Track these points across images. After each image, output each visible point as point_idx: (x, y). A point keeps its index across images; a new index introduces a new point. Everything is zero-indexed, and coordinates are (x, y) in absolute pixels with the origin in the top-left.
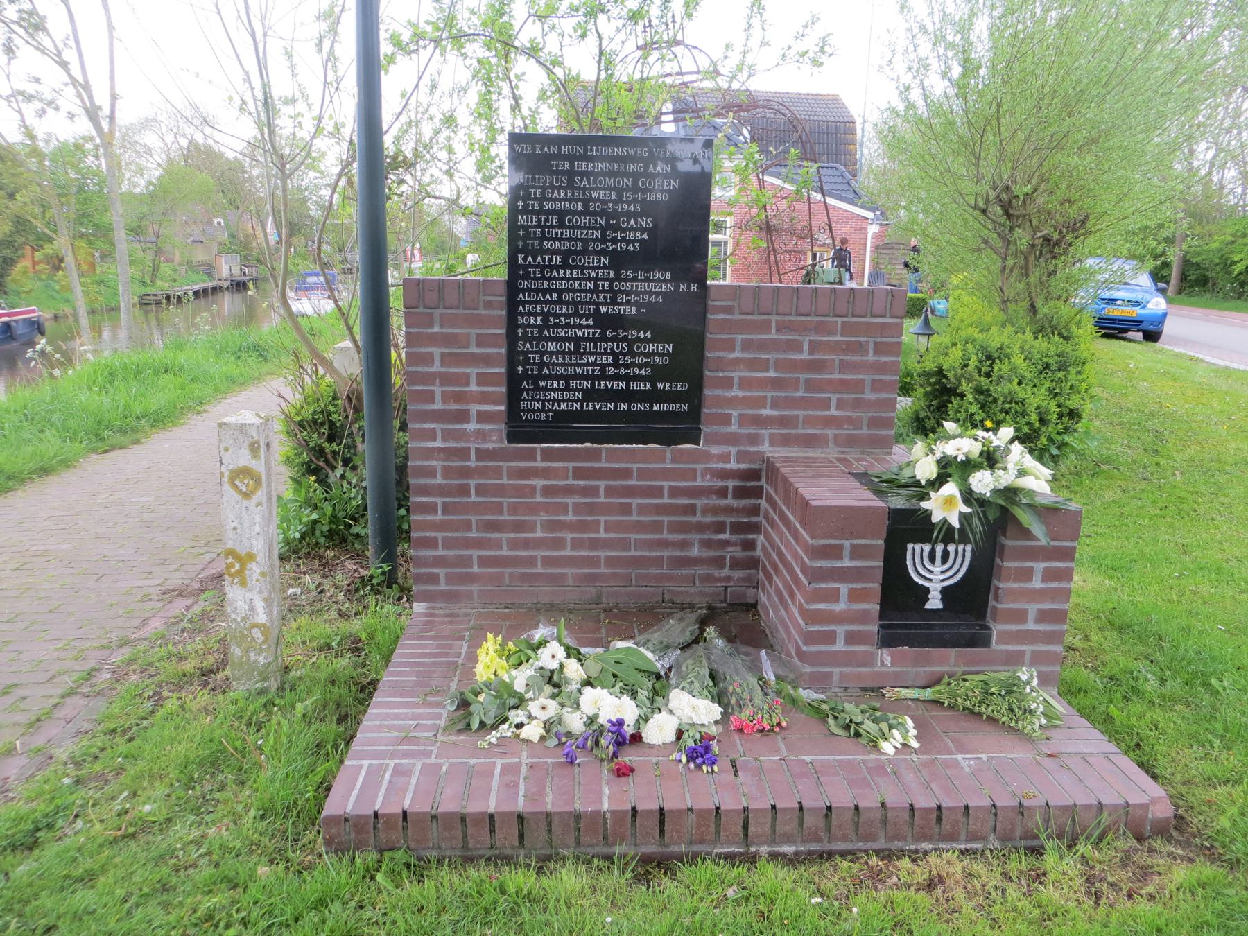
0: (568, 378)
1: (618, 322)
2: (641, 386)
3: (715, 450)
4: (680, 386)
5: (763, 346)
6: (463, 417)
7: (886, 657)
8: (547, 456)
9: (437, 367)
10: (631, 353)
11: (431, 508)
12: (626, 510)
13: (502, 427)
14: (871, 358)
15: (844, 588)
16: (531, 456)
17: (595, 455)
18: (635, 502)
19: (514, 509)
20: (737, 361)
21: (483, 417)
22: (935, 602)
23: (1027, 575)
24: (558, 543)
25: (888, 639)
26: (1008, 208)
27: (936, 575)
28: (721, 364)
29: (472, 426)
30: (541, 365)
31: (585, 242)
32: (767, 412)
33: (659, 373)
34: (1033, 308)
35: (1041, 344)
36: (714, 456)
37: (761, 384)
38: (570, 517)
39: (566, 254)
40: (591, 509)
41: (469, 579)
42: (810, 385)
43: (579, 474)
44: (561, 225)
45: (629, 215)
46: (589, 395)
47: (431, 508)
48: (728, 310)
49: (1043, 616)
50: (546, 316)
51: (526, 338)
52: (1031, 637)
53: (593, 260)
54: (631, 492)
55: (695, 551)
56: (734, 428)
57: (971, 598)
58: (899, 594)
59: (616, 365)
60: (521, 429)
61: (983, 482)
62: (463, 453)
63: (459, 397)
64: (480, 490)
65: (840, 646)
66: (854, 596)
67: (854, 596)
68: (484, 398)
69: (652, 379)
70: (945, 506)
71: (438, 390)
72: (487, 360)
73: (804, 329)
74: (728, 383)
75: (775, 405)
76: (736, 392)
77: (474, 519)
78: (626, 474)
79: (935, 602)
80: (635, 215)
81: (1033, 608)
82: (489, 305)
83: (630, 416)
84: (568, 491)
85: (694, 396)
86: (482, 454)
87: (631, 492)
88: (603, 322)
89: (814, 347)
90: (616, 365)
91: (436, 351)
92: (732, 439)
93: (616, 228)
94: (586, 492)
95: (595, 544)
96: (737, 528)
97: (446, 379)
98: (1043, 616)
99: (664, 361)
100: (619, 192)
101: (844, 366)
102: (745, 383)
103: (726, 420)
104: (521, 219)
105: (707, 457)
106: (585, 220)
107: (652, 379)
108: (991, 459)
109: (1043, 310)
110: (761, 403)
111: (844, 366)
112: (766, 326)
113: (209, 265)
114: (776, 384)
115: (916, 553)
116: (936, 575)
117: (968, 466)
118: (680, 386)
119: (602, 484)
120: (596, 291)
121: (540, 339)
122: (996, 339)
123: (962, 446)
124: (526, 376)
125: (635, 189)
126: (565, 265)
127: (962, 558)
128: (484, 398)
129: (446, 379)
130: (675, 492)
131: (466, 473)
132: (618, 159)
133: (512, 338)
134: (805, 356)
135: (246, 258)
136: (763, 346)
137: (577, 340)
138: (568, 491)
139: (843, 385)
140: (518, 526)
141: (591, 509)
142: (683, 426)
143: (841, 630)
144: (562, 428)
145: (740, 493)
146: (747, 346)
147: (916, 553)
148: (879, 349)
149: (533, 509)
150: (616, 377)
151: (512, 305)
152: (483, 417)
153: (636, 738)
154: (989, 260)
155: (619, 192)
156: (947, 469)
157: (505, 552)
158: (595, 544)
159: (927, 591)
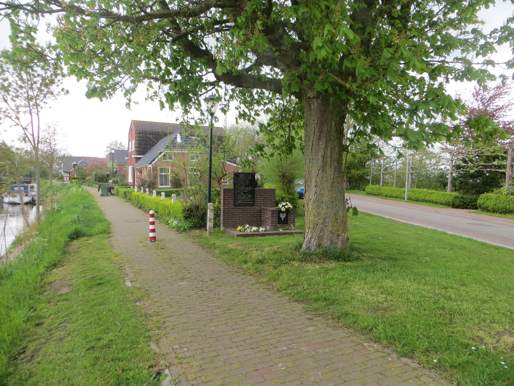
1: (246, 193)
6: (229, 204)
7: (279, 225)
25: (279, 223)
26: (283, 176)
27: (283, 216)
28: (257, 197)
34: (288, 191)
35: (290, 196)
36: (257, 208)
41: (229, 224)
57: (286, 219)
58: (280, 219)
61: (286, 207)
70: (283, 209)
85: (254, 201)
88: (244, 193)
92: (258, 206)
96: (260, 217)
97: (227, 200)
108: (287, 205)
109: (290, 191)
115: (281, 214)
116: (283, 216)
117: (285, 206)
122: (283, 195)
123: (284, 204)
127: (285, 214)
129: (227, 200)
131: (229, 211)
139: (270, 200)
142: (253, 205)
144: (240, 205)
145: (260, 212)
147: (281, 214)
151: (234, 191)
154: (281, 183)
156: (283, 206)
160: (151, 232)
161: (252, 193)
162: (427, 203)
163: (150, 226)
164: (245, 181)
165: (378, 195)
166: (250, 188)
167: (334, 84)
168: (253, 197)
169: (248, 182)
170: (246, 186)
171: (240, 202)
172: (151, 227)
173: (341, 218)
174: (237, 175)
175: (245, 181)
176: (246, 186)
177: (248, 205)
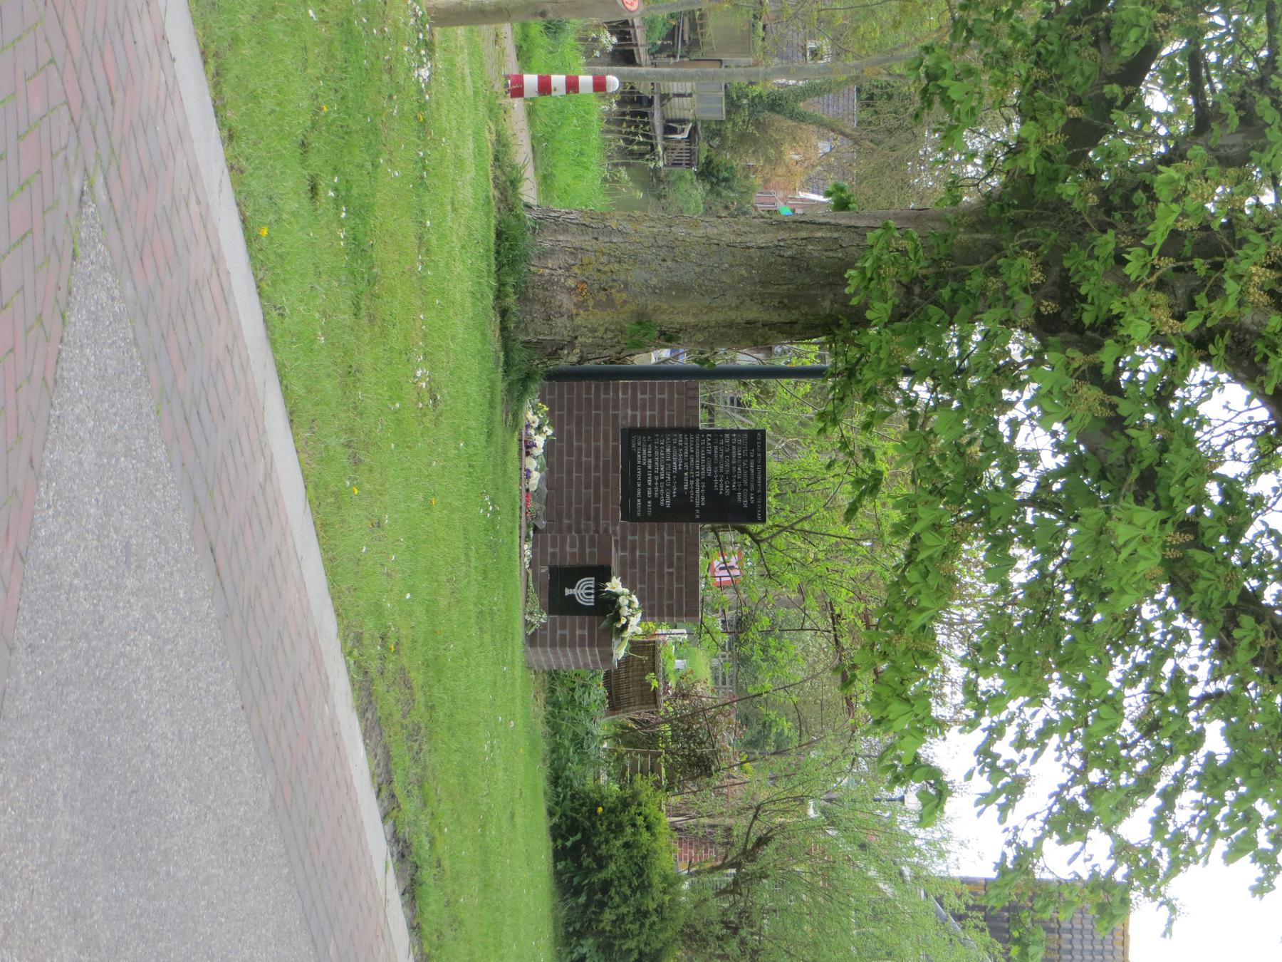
0: (653, 457)
1: (680, 481)
2: (649, 493)
3: (618, 528)
4: (650, 512)
5: (670, 548)
6: (634, 408)
7: (545, 570)
8: (615, 448)
9: (658, 396)
10: (665, 488)
11: (588, 392)
12: (588, 486)
13: (629, 425)
14: (665, 603)
15: (576, 550)
16: (615, 440)
17: (615, 471)
18: (592, 491)
19: (588, 432)
20: (662, 537)
21: (634, 417)
22: (568, 592)
23: (582, 628)
24: (570, 454)
25: (553, 570)
29: (629, 412)
30: (659, 446)
31: (718, 465)
32: (638, 553)
33: (656, 501)
37: (652, 549)
38: (584, 459)
39: (712, 456)
40: (588, 470)
42: (651, 574)
43: (606, 464)
44: (725, 454)
45: (731, 485)
46: (644, 469)
47: (588, 392)
48: (687, 531)
49: (563, 636)
50: (683, 447)
51: (672, 438)
52: (570, 444)
53: (709, 469)
54: (597, 488)
55: (566, 521)
56: (630, 538)
59: (660, 481)
60: (630, 434)
62: (616, 407)
63: (644, 406)
64: (598, 416)
65: (550, 550)
66: (573, 554)
67: (573, 554)
68: (643, 418)
69: (653, 498)
71: (647, 396)
72: (662, 419)
73: (679, 569)
74: (652, 534)
75: (642, 557)
76: (647, 538)
77: (583, 412)
78: (606, 486)
79: (568, 592)
80: (731, 488)
81: (567, 632)
82: (688, 420)
83: (635, 480)
84: (597, 458)
85: (644, 518)
86: (616, 416)
87: (597, 488)
88: (680, 473)
89: (670, 574)
90: (660, 481)
91: (666, 396)
93: (725, 479)
94: (597, 466)
95: (570, 472)
97: (652, 400)
98: (563, 636)
99: (662, 503)
100: (741, 480)
101: (661, 590)
102: (652, 542)
103: (634, 534)
104: (727, 436)
105: (615, 523)
106: (728, 465)
107: (653, 498)
110: (642, 549)
111: (661, 590)
112: (680, 550)
113: (695, 44)
114: (652, 559)
115: (589, 582)
116: (582, 591)
118: (650, 512)
119: (601, 474)
120: (695, 470)
121: (672, 444)
124: (654, 438)
125: (743, 487)
126: (707, 456)
127: (590, 601)
128: (643, 418)
129: (652, 400)
130: (597, 510)
131: (606, 409)
132: (756, 480)
133: (672, 430)
134: (666, 570)
135: (715, 131)
136: (670, 548)
137: (671, 462)
138: (597, 458)
140: (579, 433)
141: (588, 470)
142: (629, 515)
143: (558, 550)
144: (629, 456)
146: (671, 542)
148: (670, 607)
149: (588, 441)
150: (653, 481)
152: (634, 417)
153: (528, 454)
155: (741, 480)
157: (566, 427)
158: (570, 472)
159: (573, 587)
160: (540, 78)
161: (682, 511)
162: (541, 728)
163: (563, 78)
164: (729, 477)
165: (267, 328)
166: (700, 501)
167: (41, 852)
168: (660, 515)
169: (723, 488)
170: (709, 481)
171: (643, 456)
172: (558, 80)
173: (622, 277)
174: (756, 440)
175: (729, 477)
176: (709, 481)
177: (628, 492)
